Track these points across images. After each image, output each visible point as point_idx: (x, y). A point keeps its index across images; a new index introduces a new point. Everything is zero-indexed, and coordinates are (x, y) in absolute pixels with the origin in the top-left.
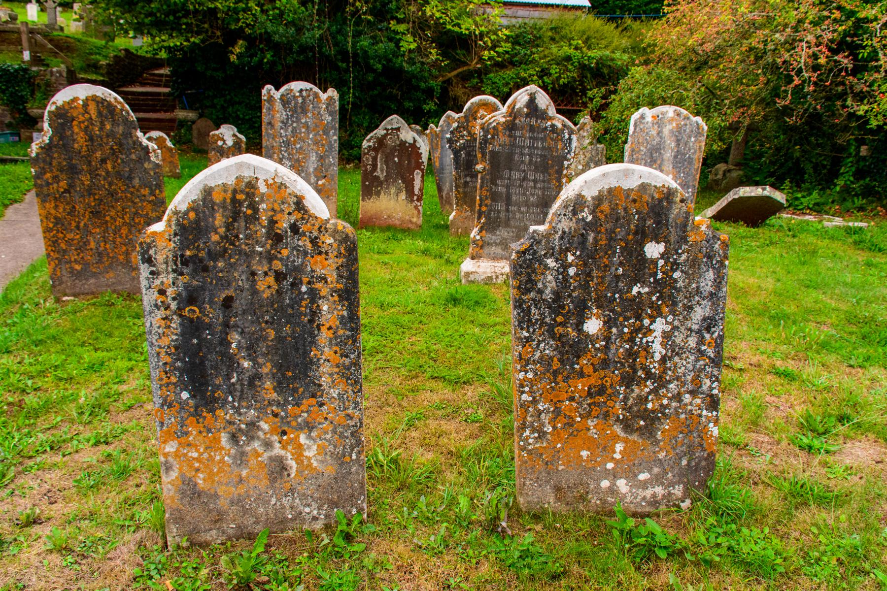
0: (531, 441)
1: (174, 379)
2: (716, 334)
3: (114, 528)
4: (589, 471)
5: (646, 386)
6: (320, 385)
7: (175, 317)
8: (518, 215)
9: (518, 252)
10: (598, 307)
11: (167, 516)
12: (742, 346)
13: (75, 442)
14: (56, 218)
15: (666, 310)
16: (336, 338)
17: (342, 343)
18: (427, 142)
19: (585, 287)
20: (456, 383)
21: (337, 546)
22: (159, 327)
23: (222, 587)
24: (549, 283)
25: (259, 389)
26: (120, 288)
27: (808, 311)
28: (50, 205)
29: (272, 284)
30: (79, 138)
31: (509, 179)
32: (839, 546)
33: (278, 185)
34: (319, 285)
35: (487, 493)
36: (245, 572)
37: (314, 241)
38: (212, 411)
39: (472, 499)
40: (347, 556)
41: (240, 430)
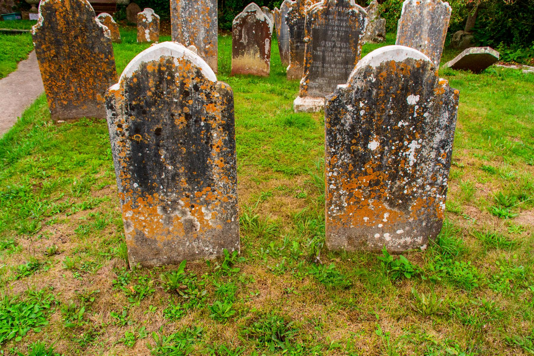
0: (335, 211)
1: (129, 176)
2: (448, 150)
3: (100, 257)
4: (368, 228)
5: (404, 180)
6: (213, 180)
7: (128, 141)
8: (329, 70)
9: (330, 101)
10: (377, 134)
11: (129, 251)
12: (464, 152)
13: (73, 208)
14: (50, 73)
15: (418, 136)
16: (221, 153)
17: (225, 156)
18: (272, 18)
19: (370, 122)
20: (291, 174)
21: (224, 269)
22: (119, 147)
23: (161, 291)
24: (348, 120)
25: (178, 182)
26: (91, 115)
27: (506, 129)
28: (46, 65)
29: (183, 121)
30: (60, 23)
31: (324, 46)
32: (511, 273)
33: (185, 61)
34: (211, 122)
35: (309, 240)
36: (174, 283)
37: (208, 95)
38: (151, 194)
39: (300, 243)
40: (230, 275)
41: (168, 205)
